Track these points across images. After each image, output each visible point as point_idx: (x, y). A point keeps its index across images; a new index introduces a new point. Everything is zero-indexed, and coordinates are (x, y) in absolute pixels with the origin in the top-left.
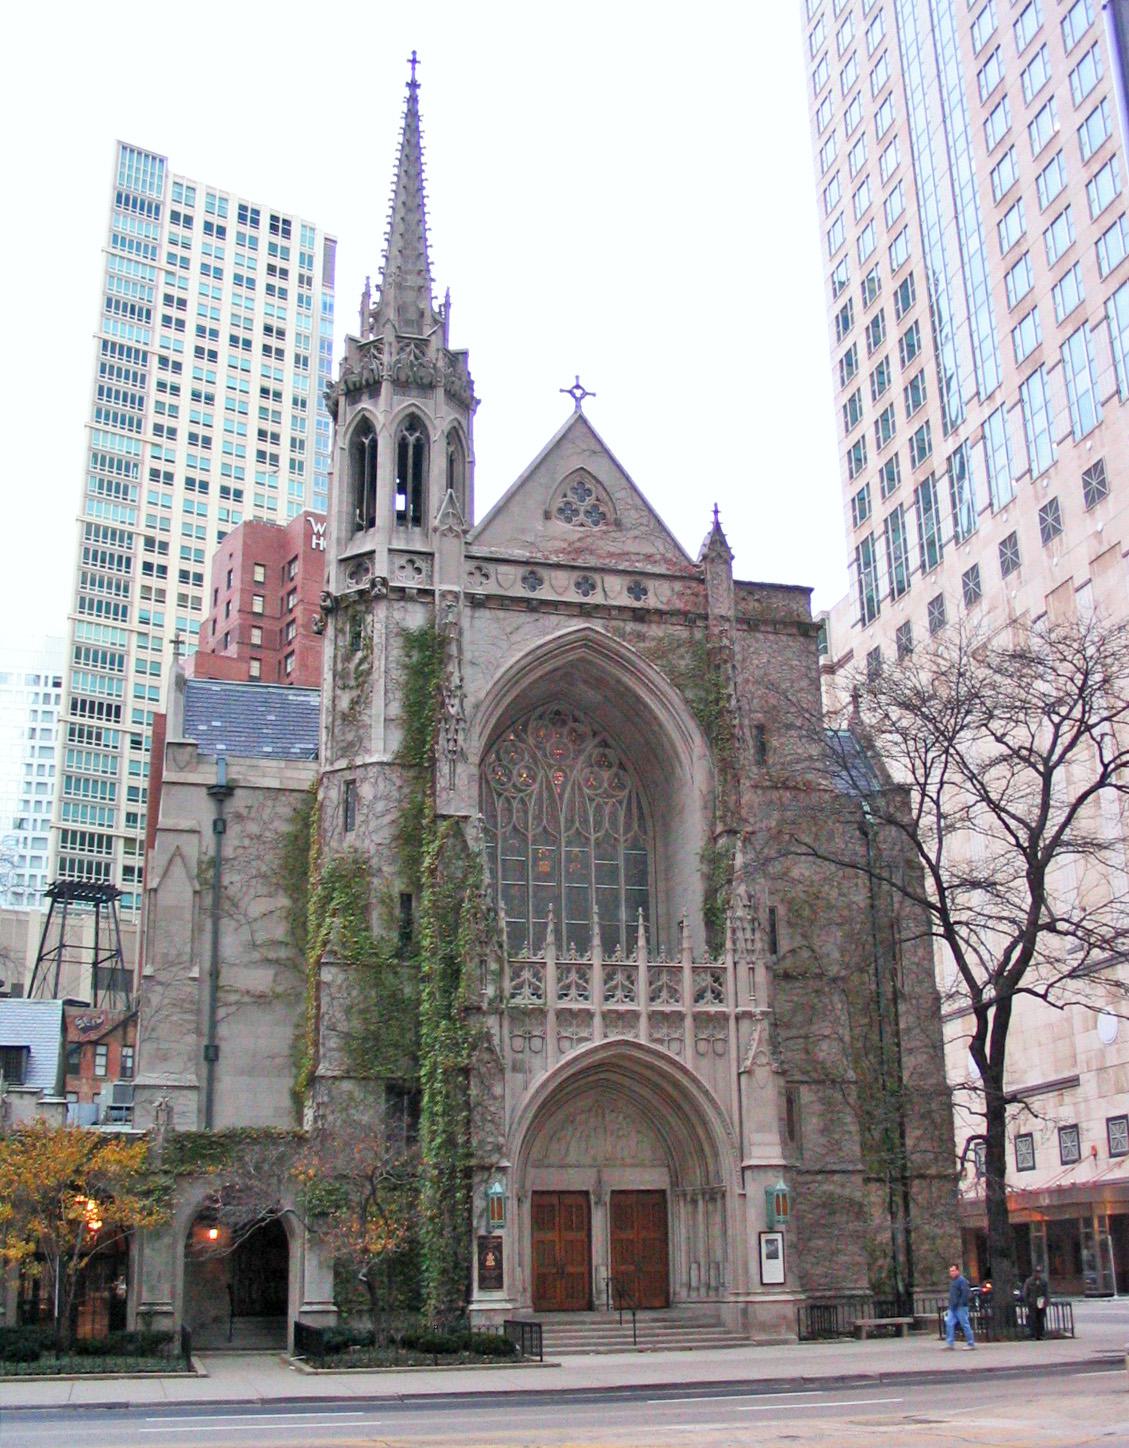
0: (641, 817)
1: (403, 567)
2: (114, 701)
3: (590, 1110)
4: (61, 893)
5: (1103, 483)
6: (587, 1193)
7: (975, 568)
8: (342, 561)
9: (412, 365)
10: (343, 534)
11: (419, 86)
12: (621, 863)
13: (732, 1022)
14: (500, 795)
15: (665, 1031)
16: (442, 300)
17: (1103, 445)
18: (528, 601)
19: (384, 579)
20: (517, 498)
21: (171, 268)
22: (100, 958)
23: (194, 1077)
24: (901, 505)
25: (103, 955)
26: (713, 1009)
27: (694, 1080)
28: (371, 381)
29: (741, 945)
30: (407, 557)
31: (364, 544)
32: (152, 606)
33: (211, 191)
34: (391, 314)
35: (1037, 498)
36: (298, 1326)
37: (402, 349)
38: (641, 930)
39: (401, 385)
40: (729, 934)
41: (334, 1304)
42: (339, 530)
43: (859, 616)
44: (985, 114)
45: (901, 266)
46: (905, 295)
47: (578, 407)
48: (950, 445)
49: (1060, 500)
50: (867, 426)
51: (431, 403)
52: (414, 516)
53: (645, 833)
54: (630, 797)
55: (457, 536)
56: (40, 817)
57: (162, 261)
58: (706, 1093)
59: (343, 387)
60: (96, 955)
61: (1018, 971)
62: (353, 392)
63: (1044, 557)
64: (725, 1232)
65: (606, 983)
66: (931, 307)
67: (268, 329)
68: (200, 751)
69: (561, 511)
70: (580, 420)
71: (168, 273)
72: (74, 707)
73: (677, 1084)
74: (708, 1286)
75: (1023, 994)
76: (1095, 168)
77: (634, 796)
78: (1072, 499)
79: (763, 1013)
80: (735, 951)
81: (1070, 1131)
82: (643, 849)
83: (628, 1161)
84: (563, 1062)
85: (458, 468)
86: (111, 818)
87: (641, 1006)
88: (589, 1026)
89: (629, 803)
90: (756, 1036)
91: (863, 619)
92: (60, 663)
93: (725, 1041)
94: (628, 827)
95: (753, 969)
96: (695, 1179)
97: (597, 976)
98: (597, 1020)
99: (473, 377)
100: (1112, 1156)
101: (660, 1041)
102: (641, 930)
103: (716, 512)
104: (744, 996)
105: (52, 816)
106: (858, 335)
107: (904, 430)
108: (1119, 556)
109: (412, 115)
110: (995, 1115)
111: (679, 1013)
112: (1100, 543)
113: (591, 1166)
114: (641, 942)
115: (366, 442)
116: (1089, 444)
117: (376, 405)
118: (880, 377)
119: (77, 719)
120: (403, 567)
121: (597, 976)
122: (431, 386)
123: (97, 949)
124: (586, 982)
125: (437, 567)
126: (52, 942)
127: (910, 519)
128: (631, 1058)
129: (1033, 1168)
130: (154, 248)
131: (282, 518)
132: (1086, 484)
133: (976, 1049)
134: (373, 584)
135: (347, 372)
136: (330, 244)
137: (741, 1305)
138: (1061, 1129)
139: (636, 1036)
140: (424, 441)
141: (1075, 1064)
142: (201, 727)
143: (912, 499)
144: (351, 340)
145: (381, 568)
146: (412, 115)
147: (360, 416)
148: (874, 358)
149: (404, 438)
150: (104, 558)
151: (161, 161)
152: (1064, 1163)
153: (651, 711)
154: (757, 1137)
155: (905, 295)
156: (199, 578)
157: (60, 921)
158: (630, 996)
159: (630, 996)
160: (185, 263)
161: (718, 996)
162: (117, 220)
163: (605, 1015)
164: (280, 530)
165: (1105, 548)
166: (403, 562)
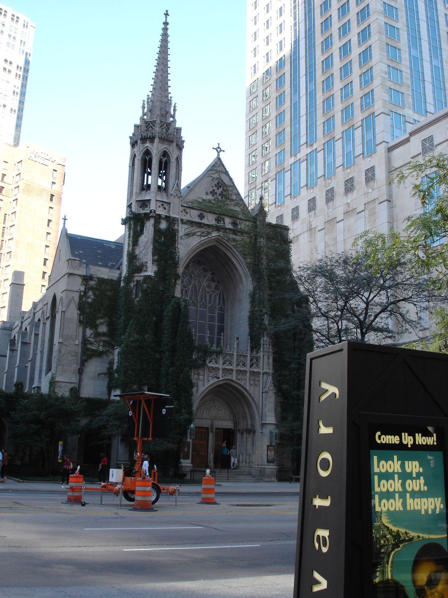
0: (223, 300)
1: (160, 207)
3: (211, 400)
5: (352, 186)
6: (208, 428)
8: (137, 201)
10: (138, 191)
12: (216, 315)
13: (261, 375)
15: (241, 376)
17: (354, 172)
18: (200, 223)
19: (155, 211)
23: (75, 379)
28: (151, 137)
30: (161, 203)
35: (325, 186)
39: (163, 140)
40: (262, 346)
41: (129, 461)
47: (218, 155)
48: (292, 160)
51: (171, 147)
55: (179, 198)
63: (326, 208)
69: (211, 192)
70: (219, 159)
74: (246, 462)
78: (340, 189)
80: (264, 351)
82: (224, 311)
83: (222, 418)
84: (209, 385)
88: (231, 374)
93: (259, 381)
94: (219, 304)
95: (269, 358)
101: (239, 379)
103: (167, 14)
104: (265, 367)
108: (355, 213)
111: (259, 372)
113: (210, 419)
115: (148, 159)
116: (349, 171)
117: (152, 145)
120: (160, 207)
122: (172, 142)
125: (171, 208)
132: (346, 185)
137: (260, 469)
140: (168, 161)
142: (76, 253)
145: (153, 206)
147: (146, 148)
165: (350, 209)
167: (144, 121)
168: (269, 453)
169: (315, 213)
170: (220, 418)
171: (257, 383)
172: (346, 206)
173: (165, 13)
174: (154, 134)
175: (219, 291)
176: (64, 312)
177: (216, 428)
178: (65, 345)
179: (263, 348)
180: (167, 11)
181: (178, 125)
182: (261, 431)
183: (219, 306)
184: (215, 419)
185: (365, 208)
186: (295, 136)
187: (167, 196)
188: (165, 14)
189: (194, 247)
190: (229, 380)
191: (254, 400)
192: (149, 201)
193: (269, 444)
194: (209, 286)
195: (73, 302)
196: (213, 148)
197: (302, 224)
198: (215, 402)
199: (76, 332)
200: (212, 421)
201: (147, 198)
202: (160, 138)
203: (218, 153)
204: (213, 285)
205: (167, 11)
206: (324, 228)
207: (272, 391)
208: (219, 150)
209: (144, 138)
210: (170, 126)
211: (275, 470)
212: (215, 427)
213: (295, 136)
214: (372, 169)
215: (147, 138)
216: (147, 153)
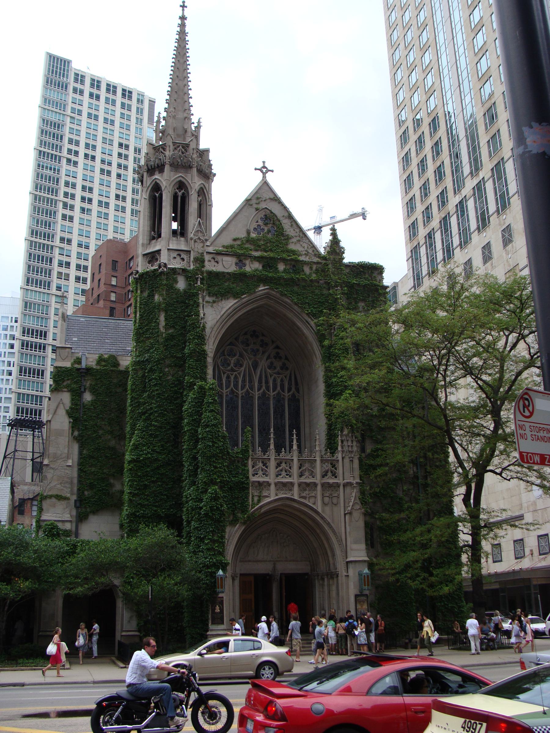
1: (175, 258)
2: (44, 329)
4: (15, 424)
7: (470, 260)
8: (144, 255)
9: (180, 157)
10: (146, 242)
11: (186, 19)
13: (341, 487)
14: (224, 373)
15: (307, 492)
16: (196, 125)
19: (165, 264)
20: (233, 223)
21: (73, 115)
22: (35, 457)
23: (69, 516)
24: (433, 229)
25: (36, 455)
26: (331, 481)
27: (323, 518)
29: (346, 449)
31: (156, 246)
32: (62, 282)
33: (93, 78)
34: (171, 132)
36: (119, 642)
37: (175, 149)
39: (176, 166)
40: (340, 444)
42: (143, 239)
43: (412, 285)
44: (473, 35)
45: (432, 111)
46: (434, 124)
47: (264, 177)
48: (457, 199)
49: (512, 225)
50: (416, 190)
52: (182, 232)
54: (291, 374)
56: (8, 387)
57: (69, 112)
58: (328, 524)
59: (146, 168)
60: (33, 455)
61: (488, 461)
62: (151, 170)
63: (504, 254)
64: (338, 594)
65: (277, 468)
66: (447, 130)
67: (121, 145)
68: (73, 351)
70: (265, 184)
71: (71, 117)
72: (24, 332)
73: (314, 520)
75: (489, 473)
77: (293, 373)
79: (357, 483)
80: (343, 451)
81: (519, 542)
85: (204, 207)
86: (42, 388)
87: (295, 479)
89: (290, 377)
90: (354, 495)
91: (414, 287)
92: (17, 312)
93: (338, 497)
95: (352, 460)
96: (322, 568)
97: (272, 464)
98: (273, 487)
99: (212, 162)
100: (540, 554)
101: (304, 498)
103: (183, 6)
104: (347, 474)
105: (14, 388)
106: (411, 145)
107: (434, 192)
109: (182, 35)
110: (475, 534)
111: (268, 482)
113: (270, 561)
114: (295, 447)
115: (157, 195)
118: (422, 164)
119: (25, 338)
120: (175, 258)
121: (272, 464)
122: (190, 167)
123: (33, 452)
126: (11, 449)
127: (438, 236)
128: (289, 506)
129: (501, 561)
130: (65, 105)
131: (127, 238)
133: (466, 500)
134: (160, 267)
135: (148, 160)
138: (515, 541)
139: (293, 495)
141: (521, 509)
143: (439, 226)
144: (150, 144)
145: (164, 258)
146: (182, 35)
148: (419, 156)
149: (176, 193)
150: (40, 258)
152: (516, 558)
153: (302, 331)
154: (355, 546)
155: (434, 124)
156: (86, 268)
157: (15, 438)
158: (265, 474)
159: (265, 474)
160: (80, 113)
161: (335, 475)
162: (47, 92)
163: (276, 484)
164: (125, 244)
166: (175, 255)
167: (152, 147)
168: (359, 606)
169: (492, 264)
170: (286, 558)
171: (335, 501)
173: (182, 4)
174: (162, 160)
175: (288, 372)
176: (50, 421)
178: (53, 469)
179: (342, 447)
180: (184, 2)
181: (202, 146)
182: (346, 574)
183: (290, 393)
186: (457, 169)
187: (187, 241)
188: (181, 6)
189: (231, 309)
190: (288, 499)
191: (331, 527)
192: (159, 251)
193: (359, 593)
194: (271, 366)
195: (61, 406)
196: (256, 169)
199: (69, 448)
200: (274, 564)
201: (157, 248)
202: (171, 165)
203: (264, 174)
204: (278, 364)
205: (184, 2)
207: (360, 511)
209: (150, 168)
210: (188, 147)
213: (457, 169)
215: (154, 168)
216: (156, 188)
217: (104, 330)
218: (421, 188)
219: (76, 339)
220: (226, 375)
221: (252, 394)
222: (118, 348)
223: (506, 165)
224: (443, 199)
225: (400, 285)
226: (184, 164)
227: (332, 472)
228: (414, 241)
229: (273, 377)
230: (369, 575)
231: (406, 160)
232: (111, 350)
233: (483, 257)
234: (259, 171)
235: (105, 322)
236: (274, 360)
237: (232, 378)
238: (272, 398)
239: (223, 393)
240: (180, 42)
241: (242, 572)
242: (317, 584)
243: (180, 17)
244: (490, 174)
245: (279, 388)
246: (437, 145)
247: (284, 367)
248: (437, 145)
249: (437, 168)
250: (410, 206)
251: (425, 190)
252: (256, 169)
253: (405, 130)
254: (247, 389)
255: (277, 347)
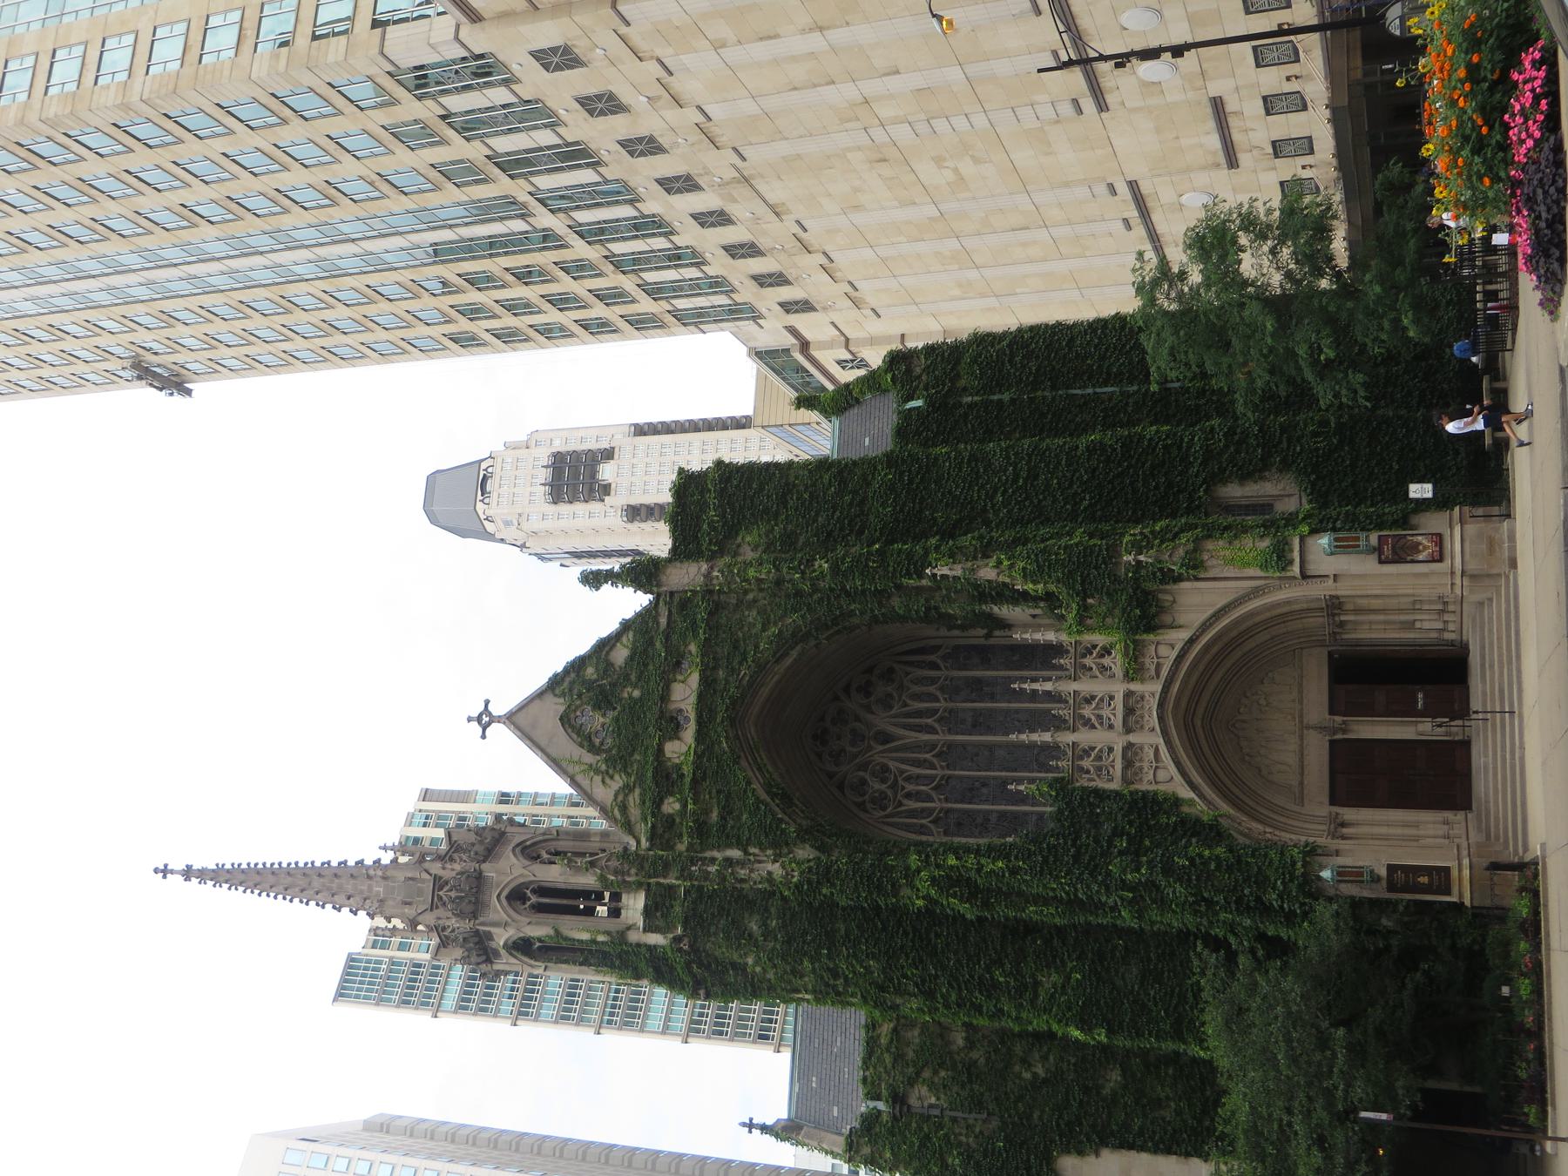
0: (922, 651)
6: (1332, 743)
11: (189, 867)
14: (900, 804)
38: (1036, 686)
47: (499, 719)
53: (939, 647)
54: (900, 662)
65: (1093, 727)
70: (511, 719)
74: (1443, 611)
76: (288, 112)
78: (619, 126)
91: (754, 319)
101: (1158, 667)
102: (1036, 686)
103: (165, 872)
106: (479, 327)
107: (566, 284)
108: (671, 79)
112: (659, 98)
113: (1301, 738)
124: (1093, 749)
136: (427, 795)
140: (536, 886)
151: (353, 960)
163: (1128, 730)
170: (1294, 701)
172: (659, 104)
177: (1332, 712)
180: (156, 871)
182: (1331, 581)
184: (1301, 716)
185: (652, 58)
188: (164, 877)
190: (1161, 705)
196: (484, 737)
197: (735, 201)
198: (1244, 721)
200: (1308, 728)
203: (493, 719)
205: (156, 871)
206: (735, 149)
208: (484, 720)
209: (484, 958)
210: (441, 878)
211: (1471, 528)
212: (1328, 717)
214: (538, 55)
216: (523, 947)
217: (817, 1040)
218: (560, 310)
219: (835, 1109)
220: (905, 801)
221: (943, 746)
222: (853, 1021)
223: (500, 150)
224: (577, 269)
225: (752, 344)
226: (474, 890)
227: (1102, 656)
228: (665, 321)
229: (909, 702)
230: (1334, 536)
231: (508, 338)
232: (857, 1037)
233: (688, 191)
234: (488, 731)
235: (801, 1040)
236: (872, 698)
237: (910, 787)
238: (951, 705)
239: (942, 809)
240: (235, 881)
241: (1326, 800)
242: (1353, 636)
243: (185, 880)
244: (521, 182)
245: (932, 689)
246: (472, 281)
247: (889, 675)
248: (472, 281)
249: (520, 279)
250: (596, 329)
251: (561, 302)
252: (484, 737)
253: (450, 339)
254: (932, 789)
255: (847, 689)
